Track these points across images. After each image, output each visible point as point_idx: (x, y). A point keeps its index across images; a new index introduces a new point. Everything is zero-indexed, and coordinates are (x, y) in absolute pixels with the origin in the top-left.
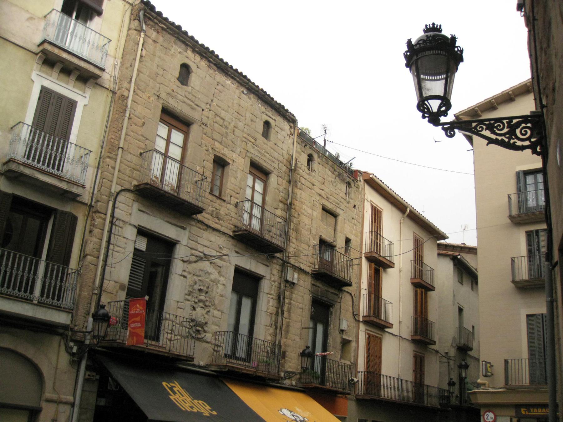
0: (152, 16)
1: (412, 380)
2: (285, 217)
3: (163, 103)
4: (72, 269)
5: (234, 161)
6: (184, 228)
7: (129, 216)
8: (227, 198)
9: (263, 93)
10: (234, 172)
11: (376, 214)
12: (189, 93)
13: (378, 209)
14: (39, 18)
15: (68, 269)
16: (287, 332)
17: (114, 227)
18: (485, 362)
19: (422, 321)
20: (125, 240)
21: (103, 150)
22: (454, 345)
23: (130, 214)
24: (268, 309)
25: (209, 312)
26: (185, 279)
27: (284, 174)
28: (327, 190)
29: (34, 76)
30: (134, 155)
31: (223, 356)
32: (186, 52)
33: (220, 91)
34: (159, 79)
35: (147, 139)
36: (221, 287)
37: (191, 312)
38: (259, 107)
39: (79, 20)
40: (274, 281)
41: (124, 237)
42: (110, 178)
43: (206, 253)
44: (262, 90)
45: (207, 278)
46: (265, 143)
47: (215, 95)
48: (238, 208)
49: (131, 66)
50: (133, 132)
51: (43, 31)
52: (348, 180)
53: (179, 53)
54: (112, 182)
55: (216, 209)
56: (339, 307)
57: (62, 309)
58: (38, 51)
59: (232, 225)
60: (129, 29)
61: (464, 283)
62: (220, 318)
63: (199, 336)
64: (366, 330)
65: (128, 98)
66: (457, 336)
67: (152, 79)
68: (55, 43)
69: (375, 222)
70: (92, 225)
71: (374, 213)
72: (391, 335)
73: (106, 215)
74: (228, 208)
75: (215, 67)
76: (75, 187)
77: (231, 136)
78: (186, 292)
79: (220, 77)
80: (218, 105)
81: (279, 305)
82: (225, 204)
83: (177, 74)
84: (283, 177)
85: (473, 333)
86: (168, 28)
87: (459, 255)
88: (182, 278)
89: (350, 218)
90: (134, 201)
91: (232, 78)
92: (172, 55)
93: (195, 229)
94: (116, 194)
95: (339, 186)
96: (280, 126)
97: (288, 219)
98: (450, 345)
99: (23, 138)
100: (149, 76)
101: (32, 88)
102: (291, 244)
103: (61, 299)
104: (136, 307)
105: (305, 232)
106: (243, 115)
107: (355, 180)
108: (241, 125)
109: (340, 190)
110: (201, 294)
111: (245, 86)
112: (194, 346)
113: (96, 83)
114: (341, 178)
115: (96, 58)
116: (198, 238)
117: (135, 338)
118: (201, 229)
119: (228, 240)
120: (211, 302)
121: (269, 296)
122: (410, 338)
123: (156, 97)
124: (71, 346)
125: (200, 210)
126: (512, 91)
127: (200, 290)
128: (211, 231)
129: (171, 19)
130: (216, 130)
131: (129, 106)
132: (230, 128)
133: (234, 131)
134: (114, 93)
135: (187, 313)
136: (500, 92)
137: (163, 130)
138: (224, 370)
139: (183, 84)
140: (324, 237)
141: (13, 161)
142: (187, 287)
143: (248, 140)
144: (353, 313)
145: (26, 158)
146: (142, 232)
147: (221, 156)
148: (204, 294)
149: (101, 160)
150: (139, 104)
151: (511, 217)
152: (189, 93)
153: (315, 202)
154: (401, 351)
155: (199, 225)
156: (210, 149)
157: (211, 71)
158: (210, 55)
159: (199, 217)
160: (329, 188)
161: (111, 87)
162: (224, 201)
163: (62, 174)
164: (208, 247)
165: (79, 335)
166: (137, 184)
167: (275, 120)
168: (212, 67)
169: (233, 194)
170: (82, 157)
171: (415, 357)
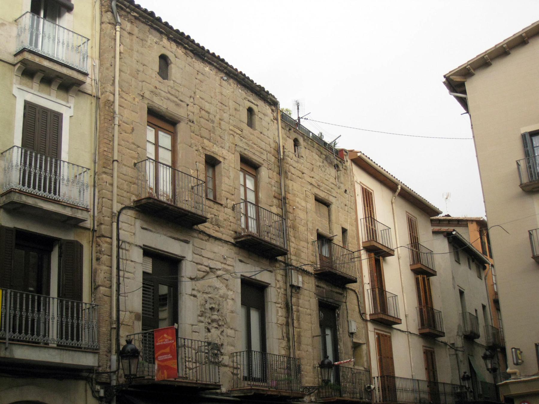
0: (125, 5)
1: (425, 379)
2: (281, 214)
3: (148, 103)
4: (86, 304)
5: (225, 158)
6: (187, 242)
7: (133, 237)
8: (223, 202)
9: (243, 77)
10: (226, 171)
11: (367, 196)
12: (172, 88)
13: (368, 190)
14: (10, 23)
15: (82, 303)
16: (300, 343)
17: (121, 250)
18: (515, 348)
19: (428, 312)
20: (133, 263)
21: (96, 165)
22: (461, 334)
23: (134, 234)
24: (278, 320)
25: (223, 332)
26: (195, 298)
27: (273, 165)
28: (317, 177)
29: (15, 91)
30: (129, 167)
31: (242, 379)
32: (162, 41)
33: (201, 81)
34: (141, 76)
35: (138, 147)
36: (230, 302)
37: (206, 334)
38: (240, 92)
39: (47, 19)
40: (280, 288)
41: (132, 261)
42: (109, 196)
43: (212, 267)
44: (241, 72)
45: (217, 294)
46: (251, 134)
47: (197, 86)
48: (235, 210)
49: (111, 66)
50: (123, 140)
51: (17, 37)
52: (336, 162)
53: (156, 43)
54: (112, 200)
55: (215, 215)
56: (345, 307)
57: (83, 350)
58: (16, 62)
59: (232, 231)
60: (102, 23)
61: (461, 262)
62: (234, 338)
64: (375, 329)
65: (114, 102)
66: (461, 324)
67: (133, 77)
68: (34, 51)
69: (367, 207)
70: (99, 251)
71: (365, 197)
72: (399, 332)
73: (111, 238)
74: (226, 212)
75: (191, 54)
76: (80, 211)
77: (218, 131)
78: (199, 313)
79: (199, 65)
80: (202, 97)
81: (288, 315)
82: (221, 208)
83: (156, 68)
84: (273, 168)
86: (141, 15)
87: (454, 230)
88: (192, 297)
89: (343, 205)
90: (135, 218)
91: (210, 63)
92: (149, 47)
93: (197, 242)
94: (117, 213)
95: (327, 171)
96: (263, 112)
97: (284, 217)
98: (456, 334)
99: (14, 163)
100: (130, 74)
101: (15, 105)
102: (291, 244)
103: (80, 339)
104: (164, 338)
105: (302, 229)
106: (227, 104)
107: (342, 161)
108: (226, 116)
109: (329, 175)
110: (214, 313)
111: (223, 70)
112: (219, 372)
113: (80, 91)
114: (329, 161)
115: (74, 60)
116: (202, 251)
117: (165, 371)
119: (230, 249)
120: (223, 320)
121: (277, 305)
122: (417, 332)
123: (141, 98)
124: (98, 389)
125: (203, 220)
126: (506, 43)
127: (212, 309)
129: (143, 6)
130: (203, 126)
131: (117, 112)
132: (216, 121)
133: (220, 124)
134: (98, 98)
135: (202, 336)
136: (494, 46)
137: (150, 134)
138: (249, 394)
139: (164, 79)
140: (321, 230)
141: (14, 191)
142: (199, 307)
143: (235, 132)
144: (360, 311)
145: (21, 185)
146: (148, 252)
147: (212, 155)
148: (216, 313)
149: (96, 176)
150: (125, 108)
151: (522, 186)
152: (172, 88)
153: (307, 192)
154: (411, 349)
155: (201, 236)
156: (200, 148)
157: (189, 59)
158: (186, 41)
159: (201, 227)
160: (318, 175)
161: (94, 92)
162: (222, 205)
163: (60, 198)
165: (105, 377)
166: (136, 199)
167: (257, 105)
168: (188, 54)
169: (229, 195)
170: (76, 176)
171: (426, 352)
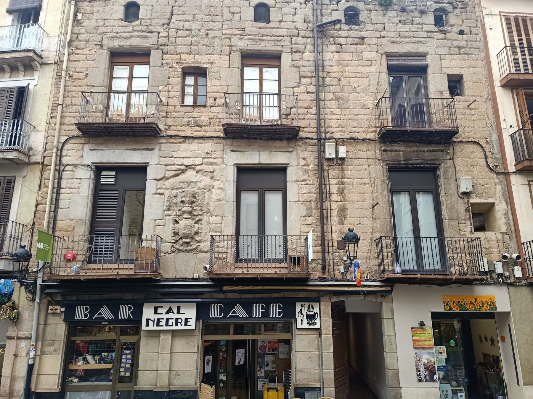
20: (78, 180)
63: (190, 248)
85: (297, 139)
93: (165, 146)
118: (176, 143)
121: (299, 183)
127: (182, 202)
128: (191, 140)
142: (165, 203)
164: (190, 158)
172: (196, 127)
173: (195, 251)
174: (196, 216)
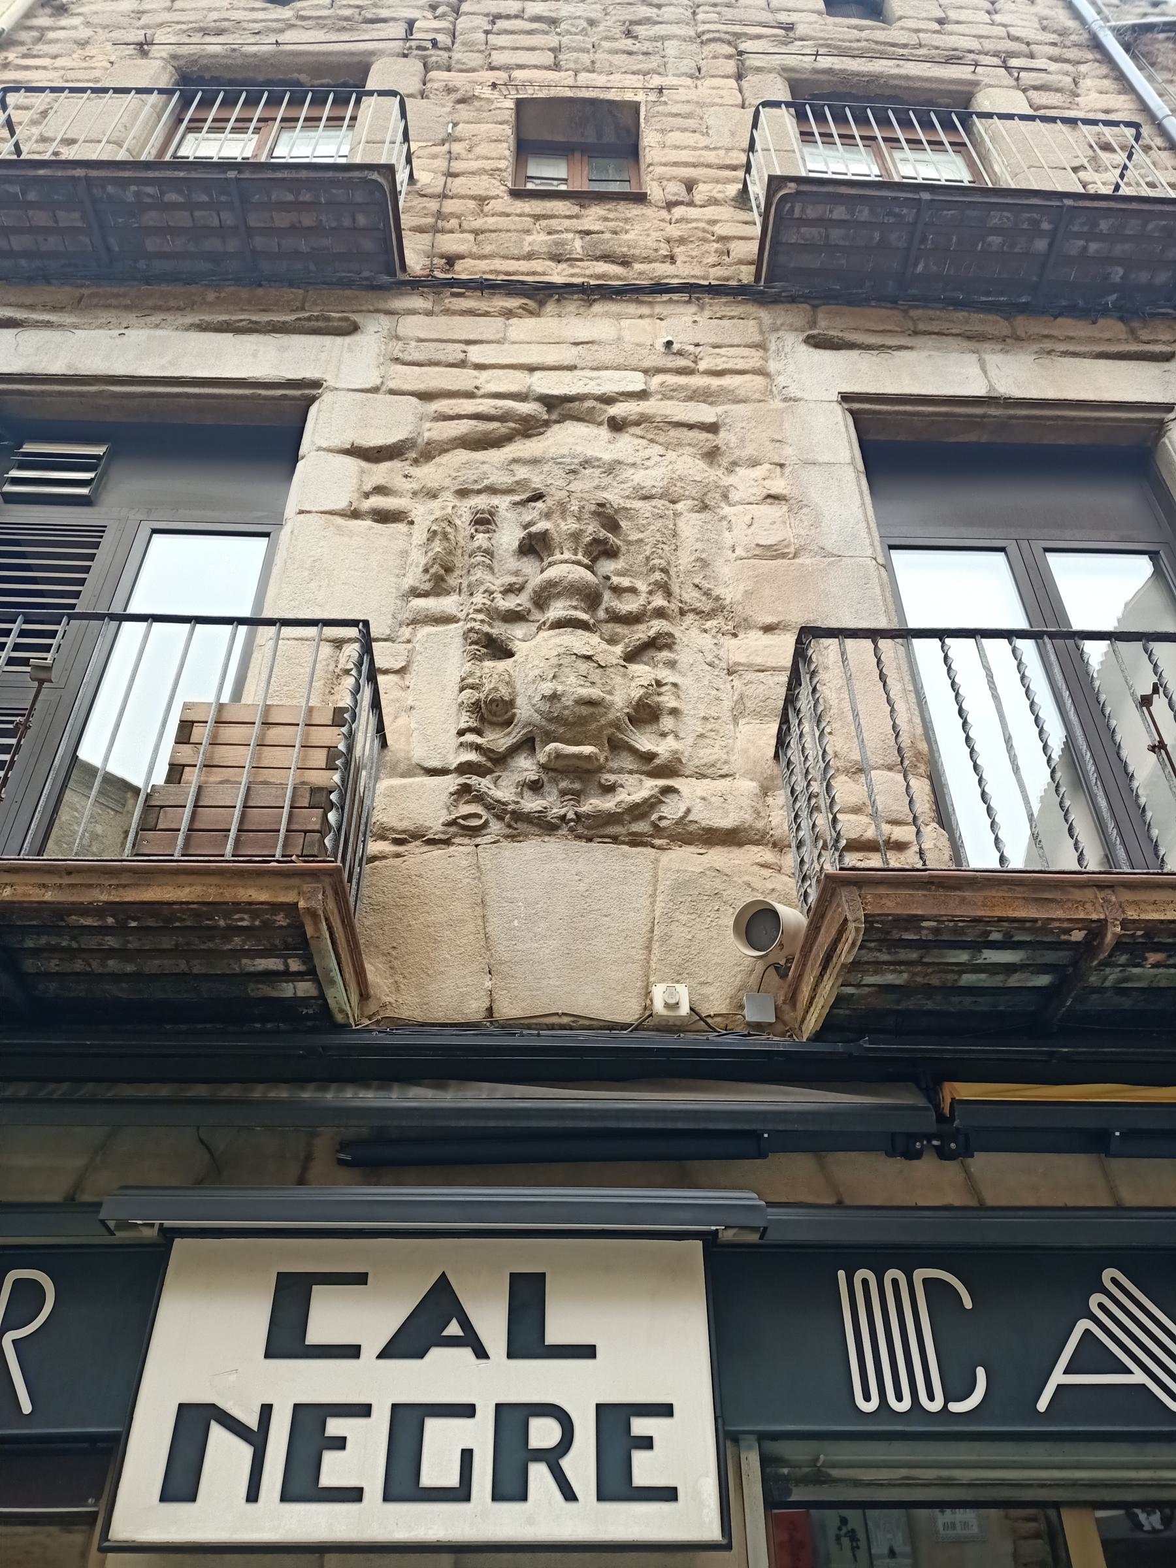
63: (594, 804)
118: (486, 314)
172: (601, 263)
173: (641, 827)
174: (632, 619)
